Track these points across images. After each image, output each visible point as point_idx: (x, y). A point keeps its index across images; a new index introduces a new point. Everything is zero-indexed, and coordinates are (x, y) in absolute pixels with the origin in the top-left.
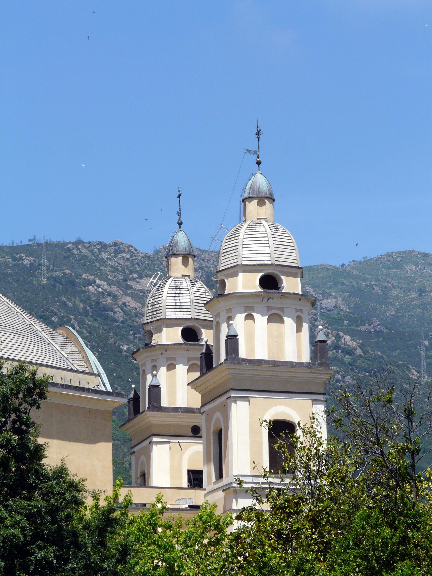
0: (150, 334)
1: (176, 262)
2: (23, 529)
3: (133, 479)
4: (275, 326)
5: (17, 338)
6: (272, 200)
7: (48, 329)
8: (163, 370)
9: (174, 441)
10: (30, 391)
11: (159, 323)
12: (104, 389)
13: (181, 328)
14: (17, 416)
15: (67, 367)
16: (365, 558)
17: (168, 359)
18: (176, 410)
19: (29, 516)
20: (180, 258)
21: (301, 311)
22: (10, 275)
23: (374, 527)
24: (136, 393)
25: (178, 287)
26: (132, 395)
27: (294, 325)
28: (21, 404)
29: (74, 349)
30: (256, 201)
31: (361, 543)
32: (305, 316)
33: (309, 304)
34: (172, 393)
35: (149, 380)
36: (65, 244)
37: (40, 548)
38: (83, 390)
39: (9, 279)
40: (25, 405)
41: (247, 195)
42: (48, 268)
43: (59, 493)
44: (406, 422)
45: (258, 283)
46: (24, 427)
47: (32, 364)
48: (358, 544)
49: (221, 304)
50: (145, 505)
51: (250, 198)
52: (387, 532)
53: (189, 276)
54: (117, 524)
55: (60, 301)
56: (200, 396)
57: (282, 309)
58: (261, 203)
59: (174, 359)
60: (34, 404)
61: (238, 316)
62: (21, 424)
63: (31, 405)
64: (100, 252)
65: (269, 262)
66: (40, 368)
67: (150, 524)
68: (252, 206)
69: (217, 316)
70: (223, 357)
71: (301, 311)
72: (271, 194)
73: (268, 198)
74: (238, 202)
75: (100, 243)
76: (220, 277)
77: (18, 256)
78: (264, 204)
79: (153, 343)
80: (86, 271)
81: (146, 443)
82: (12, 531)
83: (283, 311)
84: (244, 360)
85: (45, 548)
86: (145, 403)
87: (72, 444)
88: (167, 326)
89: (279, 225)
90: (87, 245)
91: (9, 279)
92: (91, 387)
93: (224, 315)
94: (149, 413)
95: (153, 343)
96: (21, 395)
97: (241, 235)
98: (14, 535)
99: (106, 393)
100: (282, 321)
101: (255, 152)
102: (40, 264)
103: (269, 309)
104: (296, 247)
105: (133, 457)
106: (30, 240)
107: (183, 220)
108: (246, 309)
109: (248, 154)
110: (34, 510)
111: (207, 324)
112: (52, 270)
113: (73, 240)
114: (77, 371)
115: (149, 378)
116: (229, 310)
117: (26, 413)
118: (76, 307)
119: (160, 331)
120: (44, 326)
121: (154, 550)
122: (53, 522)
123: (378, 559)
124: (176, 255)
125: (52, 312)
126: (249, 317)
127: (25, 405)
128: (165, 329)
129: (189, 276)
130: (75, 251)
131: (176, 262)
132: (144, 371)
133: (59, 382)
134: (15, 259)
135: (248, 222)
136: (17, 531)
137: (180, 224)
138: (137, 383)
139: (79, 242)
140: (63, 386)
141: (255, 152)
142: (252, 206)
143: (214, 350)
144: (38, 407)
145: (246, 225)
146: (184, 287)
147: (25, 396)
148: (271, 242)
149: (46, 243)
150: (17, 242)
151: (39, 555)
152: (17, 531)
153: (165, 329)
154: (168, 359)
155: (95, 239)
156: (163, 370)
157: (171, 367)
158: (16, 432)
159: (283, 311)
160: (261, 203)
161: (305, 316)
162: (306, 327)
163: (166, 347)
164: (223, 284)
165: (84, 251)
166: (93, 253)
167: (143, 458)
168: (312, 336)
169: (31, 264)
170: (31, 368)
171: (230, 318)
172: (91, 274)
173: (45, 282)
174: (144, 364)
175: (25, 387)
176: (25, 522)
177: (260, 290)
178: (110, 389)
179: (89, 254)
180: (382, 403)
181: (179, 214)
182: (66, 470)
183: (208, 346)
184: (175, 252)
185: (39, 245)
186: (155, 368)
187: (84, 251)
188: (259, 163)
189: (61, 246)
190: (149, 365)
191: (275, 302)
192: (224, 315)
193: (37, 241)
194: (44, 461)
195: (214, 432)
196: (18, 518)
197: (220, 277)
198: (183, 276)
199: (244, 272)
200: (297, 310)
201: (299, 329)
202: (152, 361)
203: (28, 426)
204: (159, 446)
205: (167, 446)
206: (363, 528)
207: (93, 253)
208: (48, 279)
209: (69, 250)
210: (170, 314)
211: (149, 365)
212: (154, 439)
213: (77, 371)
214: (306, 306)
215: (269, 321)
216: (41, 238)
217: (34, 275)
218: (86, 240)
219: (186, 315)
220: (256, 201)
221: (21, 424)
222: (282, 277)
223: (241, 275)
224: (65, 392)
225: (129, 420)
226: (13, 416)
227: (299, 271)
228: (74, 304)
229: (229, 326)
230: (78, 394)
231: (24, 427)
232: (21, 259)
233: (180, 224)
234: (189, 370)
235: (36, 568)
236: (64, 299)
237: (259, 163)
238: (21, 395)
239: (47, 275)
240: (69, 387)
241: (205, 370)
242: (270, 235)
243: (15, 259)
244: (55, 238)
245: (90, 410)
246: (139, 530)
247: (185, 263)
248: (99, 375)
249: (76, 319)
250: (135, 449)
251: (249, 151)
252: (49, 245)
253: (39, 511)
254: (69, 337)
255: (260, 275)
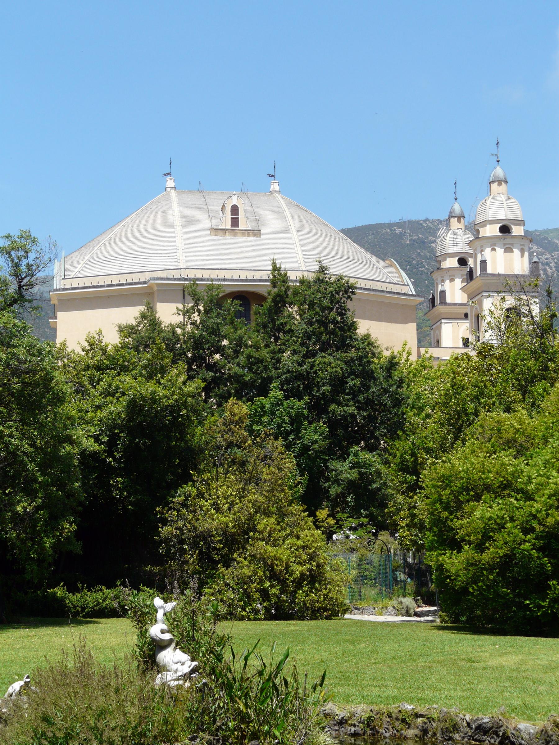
0: (440, 262)
1: (454, 221)
2: (342, 369)
3: (433, 344)
4: (508, 254)
5: (361, 266)
6: (506, 182)
7: (380, 260)
8: (447, 282)
9: (454, 322)
10: (346, 291)
11: (445, 256)
12: (411, 293)
13: (457, 258)
14: (339, 305)
15: (390, 281)
16: (517, 379)
17: (450, 276)
18: (455, 304)
19: (347, 363)
20: (456, 219)
21: (524, 245)
22: (389, 239)
23: (522, 360)
24: (433, 295)
25: (455, 235)
26: (431, 297)
27: (520, 253)
28: (341, 299)
29: (394, 272)
30: (497, 183)
31: (515, 370)
32: (526, 248)
33: (528, 241)
34: (453, 294)
35: (440, 288)
36: (419, 221)
37: (352, 380)
38: (398, 294)
39: (388, 241)
40: (344, 299)
41: (491, 180)
42: (410, 235)
43: (363, 348)
44: (547, 298)
45: (498, 230)
46: (343, 312)
47: (346, 276)
48: (512, 371)
49: (478, 243)
50: (439, 358)
51: (493, 182)
52: (531, 363)
53: (461, 229)
54: (397, 365)
55: (417, 252)
56: (467, 295)
57: (512, 245)
58: (500, 184)
59: (454, 276)
60: (349, 297)
61: (487, 249)
62: (342, 310)
63: (347, 299)
64: (438, 224)
65: (505, 218)
66: (351, 279)
67: (422, 366)
68: (495, 186)
69: (475, 250)
70: (479, 273)
71: (524, 245)
72: (505, 179)
73: (504, 181)
74: (486, 183)
75: (438, 220)
76: (477, 227)
77: (393, 229)
78: (501, 184)
79: (442, 267)
80: (430, 236)
81: (439, 323)
82: (335, 369)
83: (513, 246)
84: (491, 274)
85: (355, 379)
86: (438, 301)
87: (393, 324)
88: (449, 257)
89: (510, 197)
90: (431, 221)
91: (388, 241)
92: (403, 292)
93: (479, 249)
94: (440, 307)
95: (442, 267)
96: (341, 293)
97: (488, 202)
98: (336, 372)
99: (412, 295)
100: (512, 251)
101: (496, 155)
102: (405, 233)
103: (505, 245)
104: (520, 209)
105: (432, 332)
106: (400, 220)
107: (457, 197)
108: (491, 245)
109: (492, 156)
110: (349, 359)
111: (471, 255)
112: (412, 236)
113: (424, 219)
114: (396, 284)
115: (440, 286)
116: (482, 246)
117: (344, 304)
118: (425, 256)
119: (445, 260)
120: (377, 259)
121: (422, 380)
122: (360, 365)
123: (526, 380)
124: (454, 217)
125: (413, 258)
126: (493, 250)
127: (344, 299)
128: (448, 259)
129: (461, 229)
130: (425, 225)
131: (454, 221)
132: (437, 283)
133: (385, 290)
134: (391, 230)
135: (492, 196)
136: (338, 369)
137: (456, 199)
138: (434, 291)
139: (427, 220)
140: (387, 292)
141: (496, 155)
142: (495, 186)
143: (474, 269)
144: (351, 300)
145: (491, 197)
146: (459, 235)
147: (343, 294)
148: (506, 206)
149: (409, 221)
150: (393, 221)
151: (351, 383)
152: (338, 369)
153: (448, 259)
154: (450, 276)
155: (435, 217)
156: (447, 282)
157: (452, 280)
158: (340, 314)
159: (513, 246)
160: (500, 184)
161: (526, 248)
162: (526, 254)
163: (449, 269)
164: (478, 231)
165: (430, 224)
166: (434, 225)
167: (437, 332)
168: (530, 259)
169: (401, 233)
170: (346, 278)
171: (482, 251)
172: (434, 237)
173: (408, 242)
174: (437, 279)
175: (343, 289)
176: (343, 365)
177: (499, 234)
178: (414, 293)
179: (432, 226)
180: (531, 287)
181: (455, 193)
182: (370, 335)
183: (471, 268)
184: (453, 215)
185: (405, 222)
186: (443, 281)
187: (430, 224)
188: (498, 161)
189: (417, 222)
190: (440, 279)
191: (509, 241)
192: (479, 249)
193: (404, 220)
194: (358, 331)
195: (475, 316)
196: (339, 362)
197: (477, 227)
198: (458, 229)
199: (490, 224)
200: (521, 245)
201: (522, 256)
202: (441, 277)
203: (345, 311)
204: (446, 324)
205: (450, 325)
206: (516, 361)
207: (434, 225)
208: (410, 240)
209: (421, 224)
210: (451, 250)
211: (440, 279)
212: (443, 321)
213: (396, 284)
214: (526, 243)
215: (505, 252)
216: (406, 219)
217: (402, 239)
218: (430, 219)
219: (460, 250)
220: (497, 183)
221: (342, 310)
222: (512, 226)
223: (488, 226)
224: (388, 295)
225: (429, 311)
226: (337, 306)
227: (522, 223)
228: (425, 254)
229: (482, 255)
230: (396, 296)
231: (343, 312)
232: (395, 230)
233: (456, 199)
234: (462, 282)
235: (350, 391)
236: (419, 251)
237: (498, 161)
238: (341, 293)
239: (409, 238)
240: (390, 292)
241: (469, 281)
242: (505, 203)
243: (391, 230)
244: (414, 218)
245: (403, 305)
246: (415, 369)
247: (459, 221)
248: (408, 285)
249: (426, 262)
250: (433, 327)
251: (492, 155)
252: (410, 222)
253: (352, 359)
254: (392, 264)
255: (499, 225)
